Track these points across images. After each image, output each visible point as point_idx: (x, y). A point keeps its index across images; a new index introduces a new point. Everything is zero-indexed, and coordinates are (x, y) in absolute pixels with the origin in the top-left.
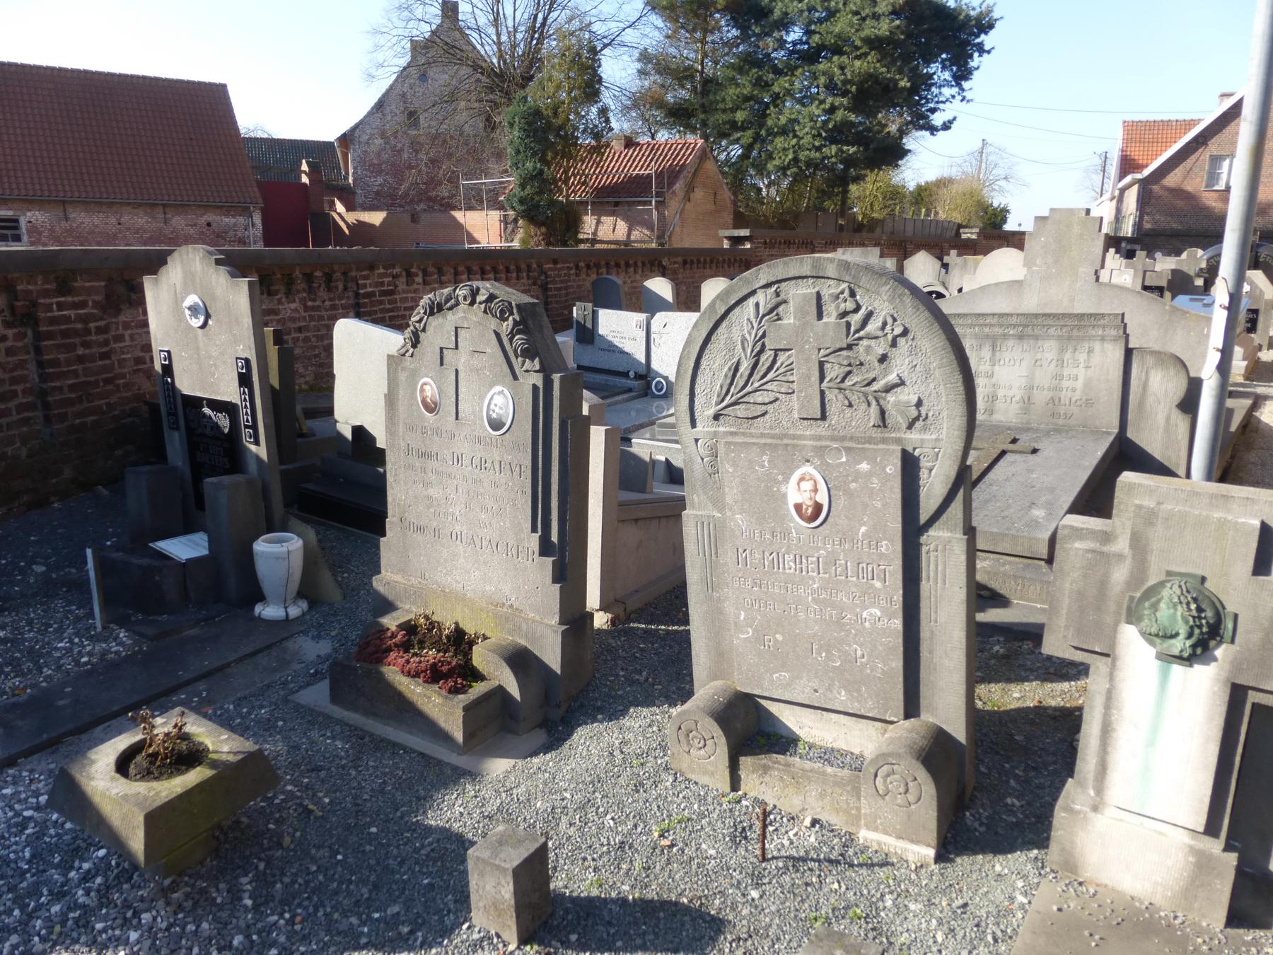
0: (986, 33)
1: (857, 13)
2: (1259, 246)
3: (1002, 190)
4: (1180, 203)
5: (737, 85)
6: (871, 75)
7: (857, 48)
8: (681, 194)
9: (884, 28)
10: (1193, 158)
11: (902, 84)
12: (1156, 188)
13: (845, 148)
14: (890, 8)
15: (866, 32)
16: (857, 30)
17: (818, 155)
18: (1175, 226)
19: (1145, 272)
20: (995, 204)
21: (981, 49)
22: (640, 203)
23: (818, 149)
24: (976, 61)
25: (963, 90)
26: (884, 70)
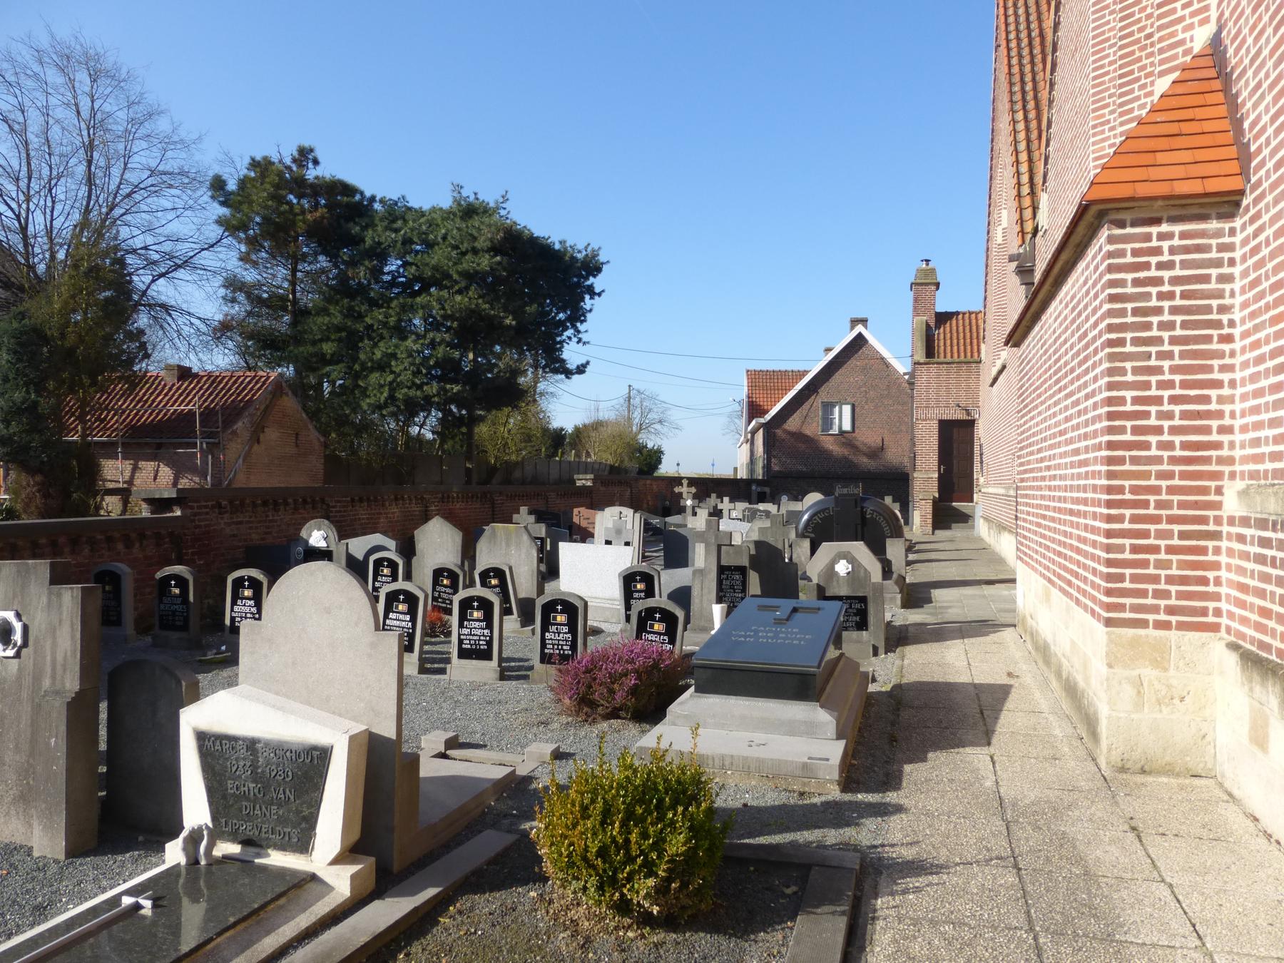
0: (595, 276)
1: (456, 247)
2: (864, 500)
3: (657, 433)
4: (802, 446)
5: (329, 315)
6: (473, 311)
7: (456, 282)
8: (246, 435)
9: (485, 262)
10: (806, 406)
11: (508, 321)
12: (779, 432)
13: (448, 386)
14: (488, 244)
15: (460, 268)
16: (455, 264)
17: (419, 393)
18: (800, 468)
19: (719, 547)
20: (650, 445)
21: (592, 293)
22: (181, 446)
23: (420, 387)
24: (588, 302)
25: (579, 332)
26: (487, 306)
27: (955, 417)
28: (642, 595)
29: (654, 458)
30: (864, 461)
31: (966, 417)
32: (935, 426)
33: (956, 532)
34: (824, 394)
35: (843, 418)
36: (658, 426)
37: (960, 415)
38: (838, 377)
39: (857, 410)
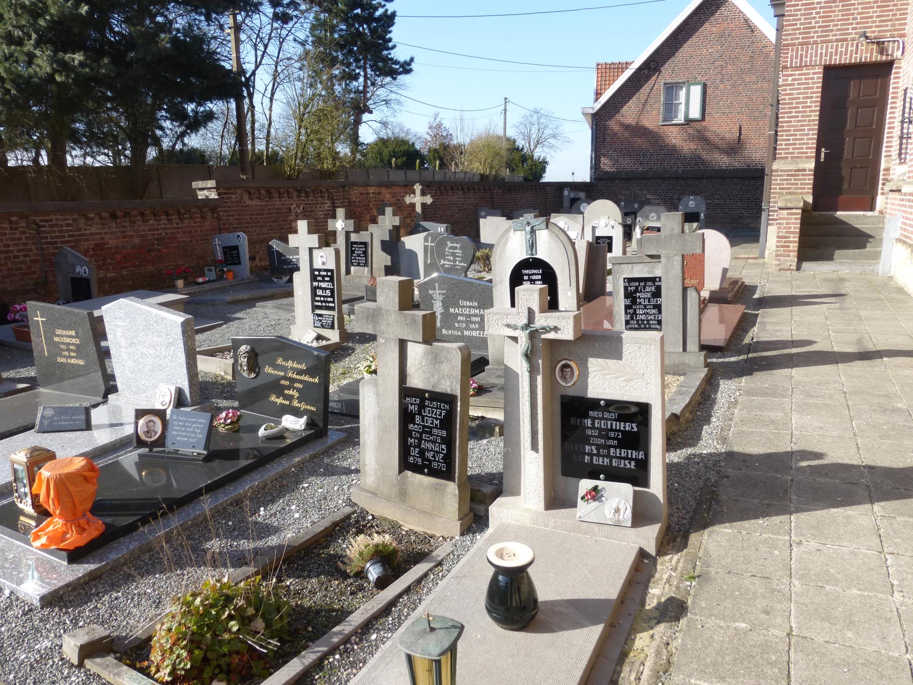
27: (855, 59)
28: (460, 318)
29: (540, 167)
30: (723, 161)
31: (877, 57)
32: (816, 78)
33: (841, 267)
34: (667, 74)
35: (690, 103)
36: (552, 141)
37: (867, 54)
38: (686, 50)
39: (709, 91)
